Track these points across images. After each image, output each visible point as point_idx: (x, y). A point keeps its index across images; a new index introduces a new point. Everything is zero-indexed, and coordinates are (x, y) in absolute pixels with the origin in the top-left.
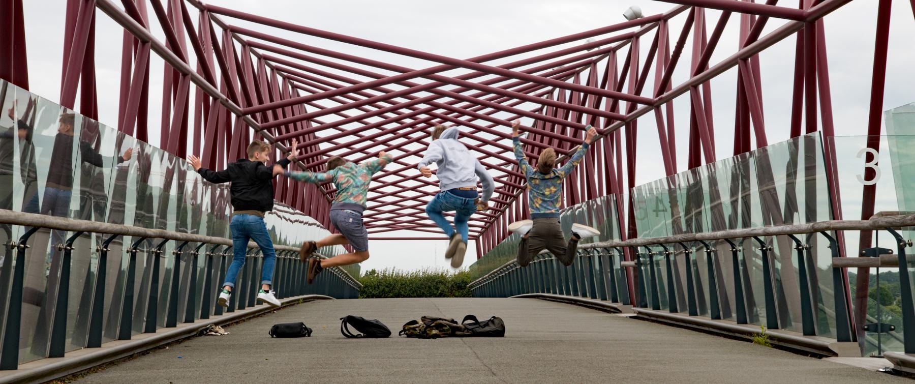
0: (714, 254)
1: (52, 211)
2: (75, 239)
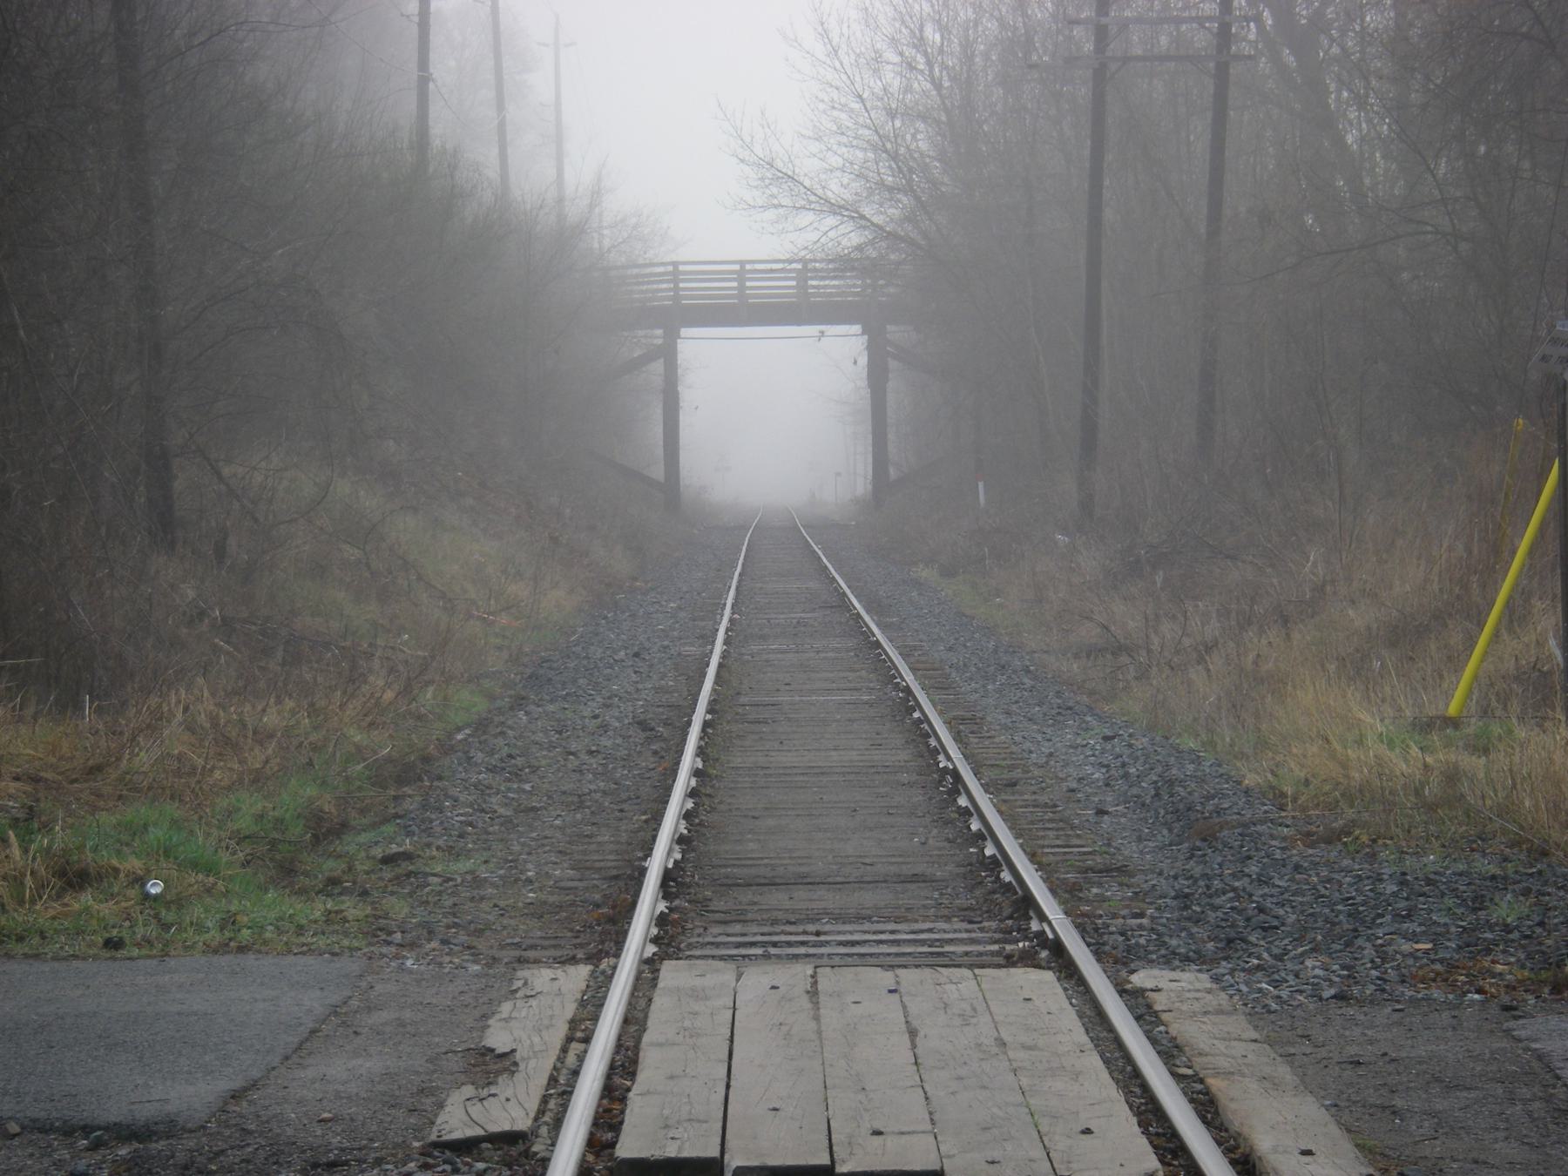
2: (420, 37)
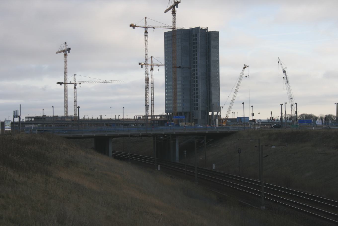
2: (168, 11)
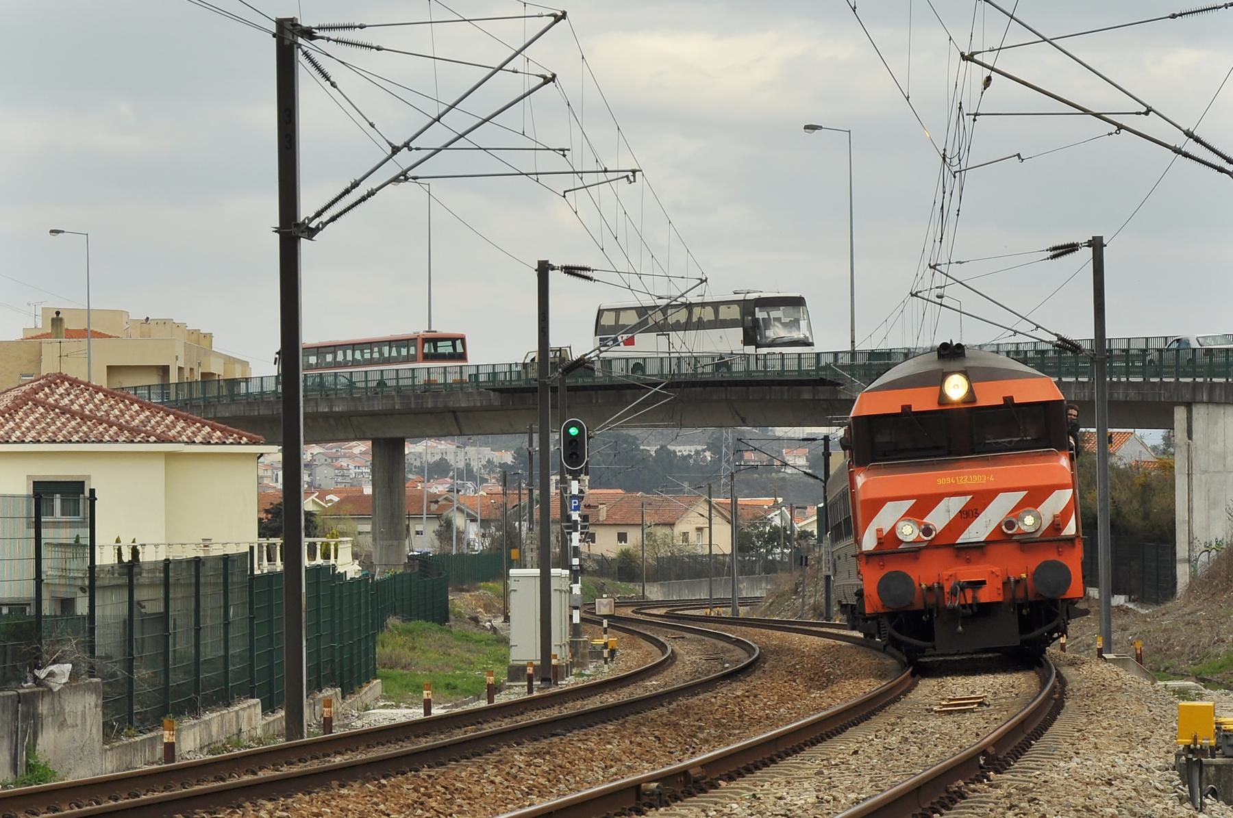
0: (541, 508)
1: (861, 639)
2: (1191, 422)
